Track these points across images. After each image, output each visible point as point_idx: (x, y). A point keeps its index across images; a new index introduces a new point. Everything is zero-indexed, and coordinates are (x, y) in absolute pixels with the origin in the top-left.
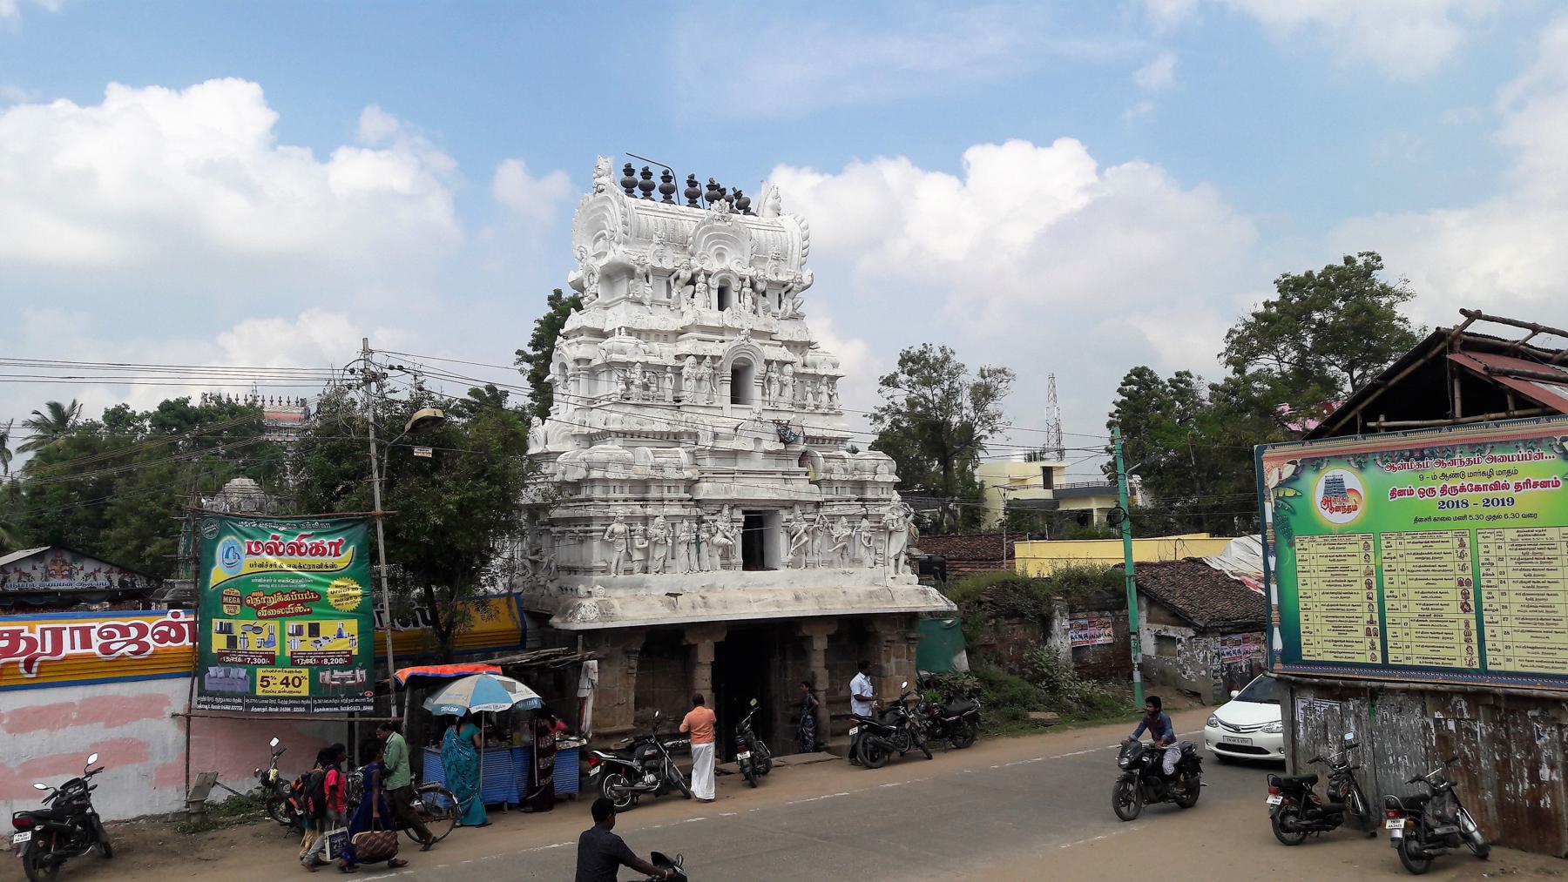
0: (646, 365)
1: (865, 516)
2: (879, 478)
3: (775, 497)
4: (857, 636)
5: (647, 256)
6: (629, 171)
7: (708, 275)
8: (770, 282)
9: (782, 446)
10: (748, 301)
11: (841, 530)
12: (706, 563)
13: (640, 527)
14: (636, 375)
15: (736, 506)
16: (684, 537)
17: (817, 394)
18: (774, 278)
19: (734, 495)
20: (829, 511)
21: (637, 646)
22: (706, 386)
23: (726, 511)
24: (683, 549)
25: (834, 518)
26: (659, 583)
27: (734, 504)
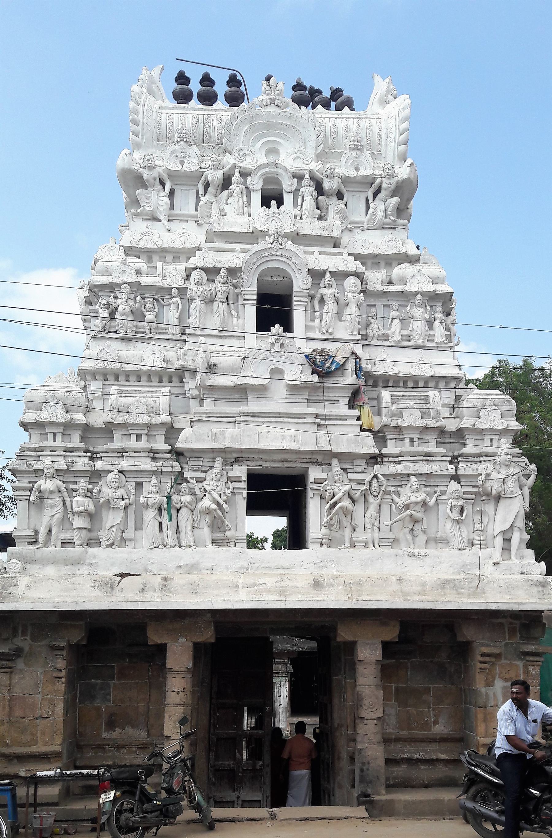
0: (137, 288)
1: (456, 478)
2: (482, 424)
3: (294, 446)
4: (432, 643)
5: (166, 161)
6: (182, 79)
7: (245, 174)
8: (346, 180)
9: (315, 378)
10: (309, 202)
11: (412, 493)
12: (187, 535)
13: (82, 485)
14: (123, 304)
15: (237, 461)
16: (154, 499)
17: (405, 321)
18: (351, 173)
19: (227, 443)
20: (391, 469)
21: (77, 636)
22: (220, 307)
23: (218, 464)
24: (150, 515)
25: (400, 479)
26: (107, 560)
27: (231, 457)
